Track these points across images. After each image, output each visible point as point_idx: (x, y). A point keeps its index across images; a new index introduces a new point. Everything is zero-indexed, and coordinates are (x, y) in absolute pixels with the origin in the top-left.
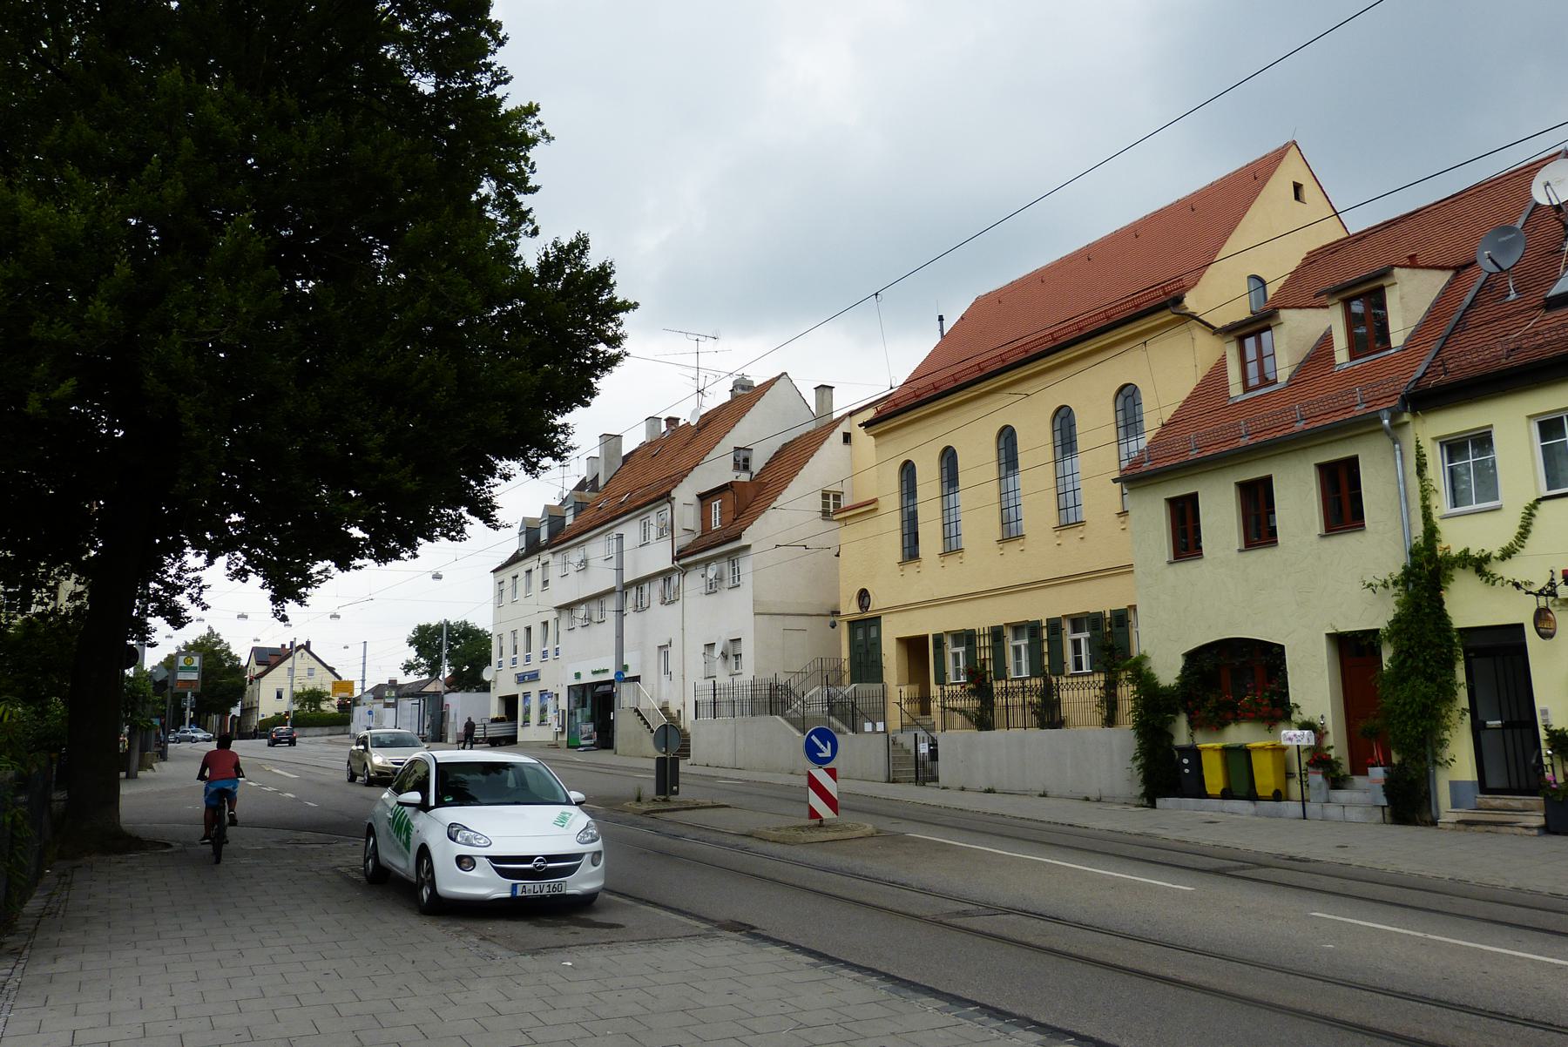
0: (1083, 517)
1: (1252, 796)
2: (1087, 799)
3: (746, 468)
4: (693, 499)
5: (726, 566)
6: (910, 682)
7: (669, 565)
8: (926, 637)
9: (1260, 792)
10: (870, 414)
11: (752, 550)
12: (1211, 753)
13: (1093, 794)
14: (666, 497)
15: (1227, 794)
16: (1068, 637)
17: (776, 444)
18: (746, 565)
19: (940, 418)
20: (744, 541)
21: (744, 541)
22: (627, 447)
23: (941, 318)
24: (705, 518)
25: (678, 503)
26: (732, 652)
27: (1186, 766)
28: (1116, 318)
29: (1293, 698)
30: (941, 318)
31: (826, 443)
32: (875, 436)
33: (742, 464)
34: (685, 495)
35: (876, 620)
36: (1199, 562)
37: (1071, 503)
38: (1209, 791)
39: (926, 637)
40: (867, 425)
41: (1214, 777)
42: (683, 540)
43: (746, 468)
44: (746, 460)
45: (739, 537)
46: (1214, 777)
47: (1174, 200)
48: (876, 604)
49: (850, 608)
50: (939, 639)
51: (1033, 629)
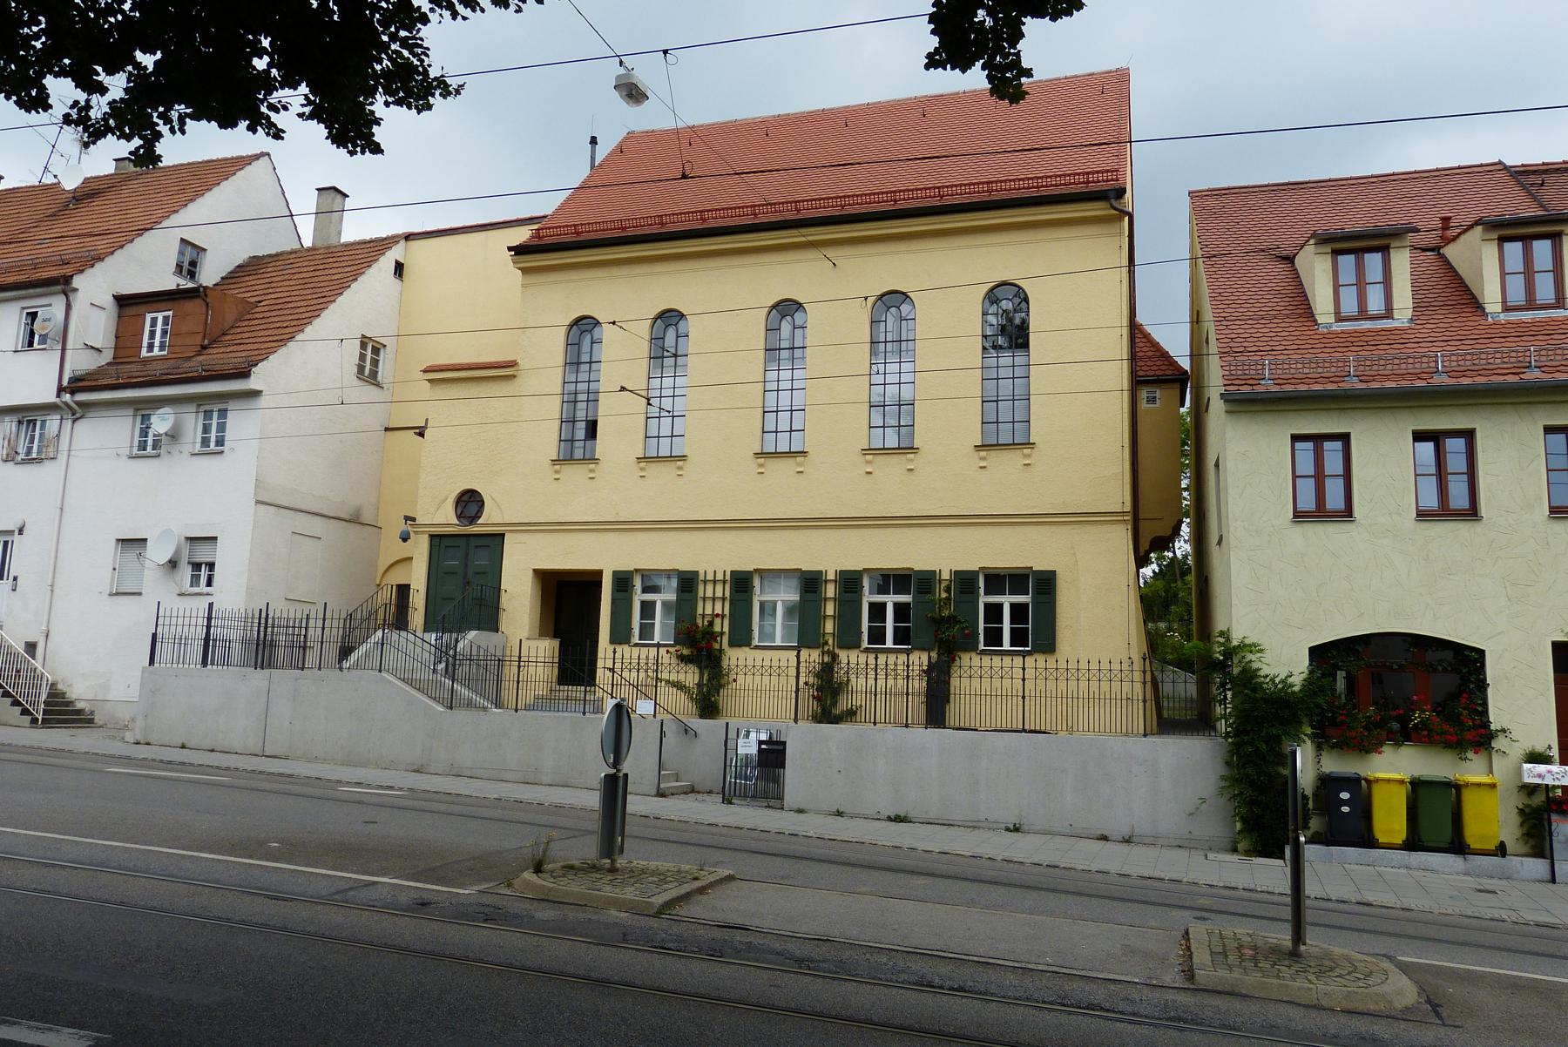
0: (808, 442)
1: (1458, 846)
2: (1104, 838)
3: (192, 275)
4: (108, 301)
5: (192, 423)
6: (543, 634)
7: (50, 397)
8: (599, 573)
9: (1472, 841)
10: (522, 235)
11: (264, 401)
12: (1395, 788)
13: (1117, 827)
14: (62, 284)
15: (1413, 843)
16: (868, 597)
17: (241, 257)
18: (241, 424)
19: (615, 271)
20: (253, 383)
21: (253, 383)
22: (375, 129)
23: (594, 141)
24: (126, 339)
25: (80, 301)
26: (196, 561)
27: (1345, 803)
28: (670, 228)
29: (1496, 719)
30: (594, 141)
31: (375, 267)
32: (525, 271)
33: (189, 268)
34: (97, 288)
35: (495, 541)
36: (1476, 524)
37: (665, 431)
38: (1381, 835)
39: (599, 573)
40: (519, 250)
41: (1390, 819)
42: (80, 362)
43: (192, 275)
44: (193, 264)
45: (245, 375)
46: (1390, 819)
47: (820, 107)
48: (491, 517)
49: (445, 517)
50: (623, 582)
51: (811, 583)
